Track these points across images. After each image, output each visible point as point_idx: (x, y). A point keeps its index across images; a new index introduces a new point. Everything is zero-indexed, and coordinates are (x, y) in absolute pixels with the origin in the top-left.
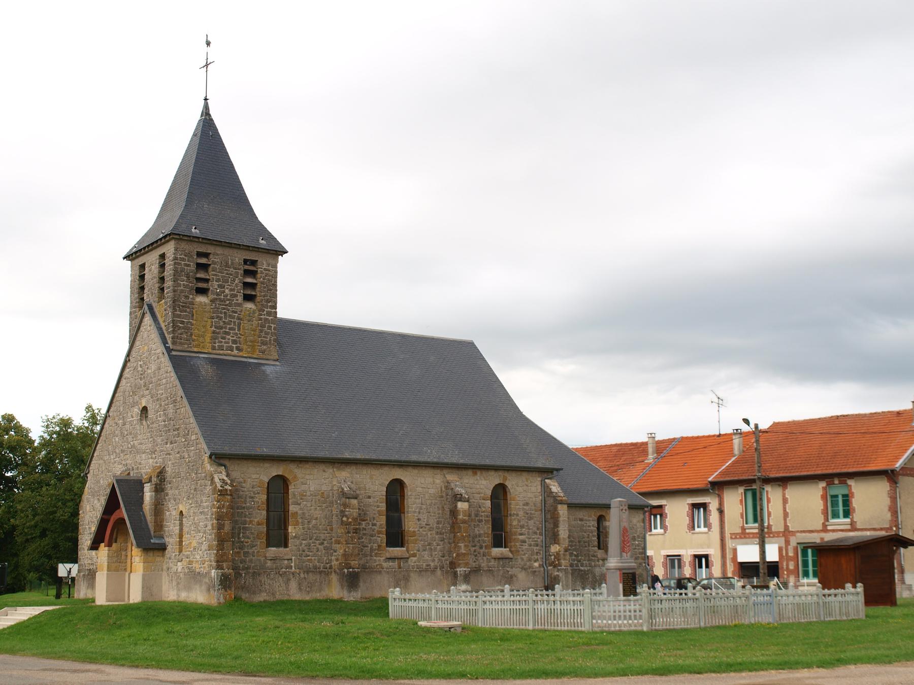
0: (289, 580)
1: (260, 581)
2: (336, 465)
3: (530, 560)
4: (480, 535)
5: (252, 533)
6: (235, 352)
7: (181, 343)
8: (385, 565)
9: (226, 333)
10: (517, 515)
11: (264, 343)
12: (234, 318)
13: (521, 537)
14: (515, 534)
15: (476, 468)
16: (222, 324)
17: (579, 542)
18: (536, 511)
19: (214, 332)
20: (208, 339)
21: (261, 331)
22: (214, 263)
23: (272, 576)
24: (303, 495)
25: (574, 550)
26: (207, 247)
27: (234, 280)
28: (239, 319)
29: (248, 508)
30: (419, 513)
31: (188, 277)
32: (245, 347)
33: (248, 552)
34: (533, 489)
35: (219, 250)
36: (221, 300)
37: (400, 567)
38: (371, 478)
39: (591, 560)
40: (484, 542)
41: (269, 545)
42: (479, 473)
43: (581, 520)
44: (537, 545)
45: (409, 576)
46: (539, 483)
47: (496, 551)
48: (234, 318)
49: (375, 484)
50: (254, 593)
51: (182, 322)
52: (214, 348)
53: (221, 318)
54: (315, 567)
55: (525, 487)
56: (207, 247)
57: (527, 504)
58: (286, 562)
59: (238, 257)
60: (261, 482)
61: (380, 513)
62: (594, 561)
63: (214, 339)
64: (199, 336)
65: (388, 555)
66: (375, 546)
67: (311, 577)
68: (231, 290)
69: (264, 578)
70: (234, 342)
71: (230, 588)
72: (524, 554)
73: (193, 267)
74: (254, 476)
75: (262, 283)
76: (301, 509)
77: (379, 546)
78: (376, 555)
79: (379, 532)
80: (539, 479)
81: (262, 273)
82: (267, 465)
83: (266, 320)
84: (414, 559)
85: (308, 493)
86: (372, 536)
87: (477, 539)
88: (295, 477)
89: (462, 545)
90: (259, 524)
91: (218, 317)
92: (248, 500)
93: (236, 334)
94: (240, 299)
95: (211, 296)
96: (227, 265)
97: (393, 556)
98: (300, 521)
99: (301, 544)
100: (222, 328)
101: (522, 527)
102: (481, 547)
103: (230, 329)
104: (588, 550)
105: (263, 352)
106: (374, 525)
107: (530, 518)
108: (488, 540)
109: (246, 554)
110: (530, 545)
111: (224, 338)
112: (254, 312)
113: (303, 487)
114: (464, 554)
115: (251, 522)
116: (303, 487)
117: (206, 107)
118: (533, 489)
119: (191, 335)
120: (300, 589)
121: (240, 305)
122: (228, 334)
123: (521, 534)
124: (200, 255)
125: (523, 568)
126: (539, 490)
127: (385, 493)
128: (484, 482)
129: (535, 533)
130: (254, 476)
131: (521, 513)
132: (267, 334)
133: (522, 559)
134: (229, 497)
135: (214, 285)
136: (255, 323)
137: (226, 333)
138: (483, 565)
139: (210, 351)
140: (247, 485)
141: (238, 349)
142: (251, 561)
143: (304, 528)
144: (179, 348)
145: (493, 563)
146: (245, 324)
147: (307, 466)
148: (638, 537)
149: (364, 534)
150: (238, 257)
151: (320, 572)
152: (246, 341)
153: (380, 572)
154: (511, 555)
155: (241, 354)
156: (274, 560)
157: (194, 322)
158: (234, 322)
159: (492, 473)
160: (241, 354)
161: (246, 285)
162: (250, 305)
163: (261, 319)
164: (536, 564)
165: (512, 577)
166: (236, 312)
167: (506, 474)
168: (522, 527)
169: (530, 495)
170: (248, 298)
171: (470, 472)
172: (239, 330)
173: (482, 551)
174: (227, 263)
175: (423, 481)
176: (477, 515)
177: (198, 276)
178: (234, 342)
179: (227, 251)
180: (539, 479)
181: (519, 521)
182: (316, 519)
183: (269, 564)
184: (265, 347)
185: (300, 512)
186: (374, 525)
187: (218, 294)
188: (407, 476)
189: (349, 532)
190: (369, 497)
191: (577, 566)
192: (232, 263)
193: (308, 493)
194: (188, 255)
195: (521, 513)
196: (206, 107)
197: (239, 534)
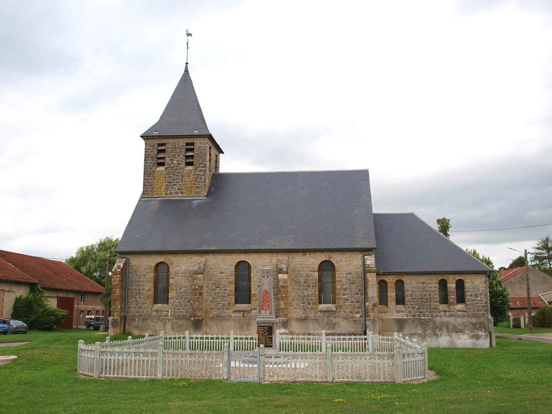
0: (165, 323)
1: (148, 324)
2: (199, 254)
3: (352, 312)
4: (308, 296)
5: (144, 296)
6: (180, 195)
7: (148, 194)
8: (233, 315)
9: (174, 185)
10: (341, 281)
11: (197, 188)
12: (179, 176)
13: (344, 297)
14: (339, 294)
15: (304, 251)
16: (171, 180)
17: (421, 299)
18: (357, 278)
19: (167, 185)
20: (163, 190)
21: (196, 181)
22: (168, 148)
23: (155, 321)
24: (176, 273)
25: (416, 305)
26: (179, 143)
27: (179, 155)
28: (182, 176)
29: (142, 282)
30: (259, 284)
31: (152, 157)
32: (186, 191)
33: (140, 307)
34: (355, 263)
35: (171, 141)
36: (171, 167)
37: (244, 317)
38: (224, 261)
39: (433, 312)
40: (311, 300)
41: (155, 302)
42: (307, 254)
43: (423, 283)
44: (359, 302)
45: (250, 322)
46: (360, 259)
47: (323, 306)
48: (179, 176)
49: (225, 265)
50: (143, 330)
51: (149, 182)
52: (166, 194)
53: (171, 177)
54: (184, 316)
55: (348, 262)
56: (179, 143)
57: (350, 274)
58: (165, 313)
59: (182, 142)
60: (150, 266)
61: (230, 283)
62: (436, 312)
63: (166, 189)
64: (158, 188)
65: (235, 309)
66: (226, 303)
67: (181, 322)
68: (177, 161)
69: (149, 322)
70: (179, 189)
71: (117, 327)
72: (347, 308)
73: (155, 152)
74: (146, 263)
75: (196, 154)
76: (175, 281)
77: (229, 303)
78: (227, 309)
79: (229, 295)
80: (361, 256)
81: (197, 149)
82: (154, 256)
83: (199, 174)
84: (255, 311)
85: (180, 272)
86: (223, 297)
87: (306, 298)
88: (172, 263)
89: (282, 303)
90: (148, 290)
91: (169, 177)
92: (142, 277)
93: (180, 185)
94: (183, 165)
95: (166, 166)
96: (175, 148)
97: (238, 309)
98: (174, 288)
99: (175, 302)
100: (171, 182)
101: (346, 289)
102: (309, 304)
103: (176, 182)
104: (430, 305)
105: (197, 193)
106: (225, 290)
107: (352, 283)
108: (316, 299)
109: (140, 308)
110: (352, 302)
111: (173, 188)
112: (191, 171)
113: (177, 268)
114: (284, 309)
115: (143, 289)
116: (177, 268)
117: (186, 71)
118: (355, 263)
119: (154, 188)
120: (173, 329)
121: (182, 168)
122: (175, 185)
123: (344, 295)
124: (159, 145)
125: (346, 318)
126: (361, 264)
127: (233, 270)
128: (312, 260)
129: (358, 294)
130: (146, 263)
131: (344, 280)
132: (199, 182)
133: (345, 312)
134: (119, 276)
135: (167, 160)
136: (192, 177)
137: (174, 185)
138: (310, 316)
139: (164, 195)
140: (142, 269)
141: (181, 193)
142: (143, 312)
143: (177, 293)
144: (146, 196)
145: (319, 314)
146: (186, 179)
147: (179, 256)
148: (481, 294)
149: (218, 296)
150: (182, 142)
151: (187, 319)
152: (186, 188)
153: (229, 320)
154: (335, 309)
155: (183, 195)
156: (157, 311)
157: (155, 181)
158: (179, 179)
159: (319, 254)
160: (183, 195)
161: (187, 157)
162: (190, 168)
163: (196, 175)
164: (358, 315)
165: (334, 324)
166: (180, 173)
167: (331, 254)
168: (346, 289)
169: (351, 267)
170: (188, 164)
171: (300, 254)
172: (182, 182)
173: (310, 306)
174: (175, 147)
175: (262, 261)
176: (305, 282)
177: (159, 156)
178: (179, 189)
179: (175, 141)
180: (361, 256)
181: (342, 285)
182: (185, 287)
183: (154, 313)
184: (198, 190)
185: (174, 283)
186: (225, 290)
187: (169, 165)
188: (250, 259)
189: (195, 295)
190: (222, 273)
191: (419, 316)
192: (178, 146)
193: (180, 272)
194: (153, 146)
195: (344, 280)
196: (186, 71)
197: (136, 296)
